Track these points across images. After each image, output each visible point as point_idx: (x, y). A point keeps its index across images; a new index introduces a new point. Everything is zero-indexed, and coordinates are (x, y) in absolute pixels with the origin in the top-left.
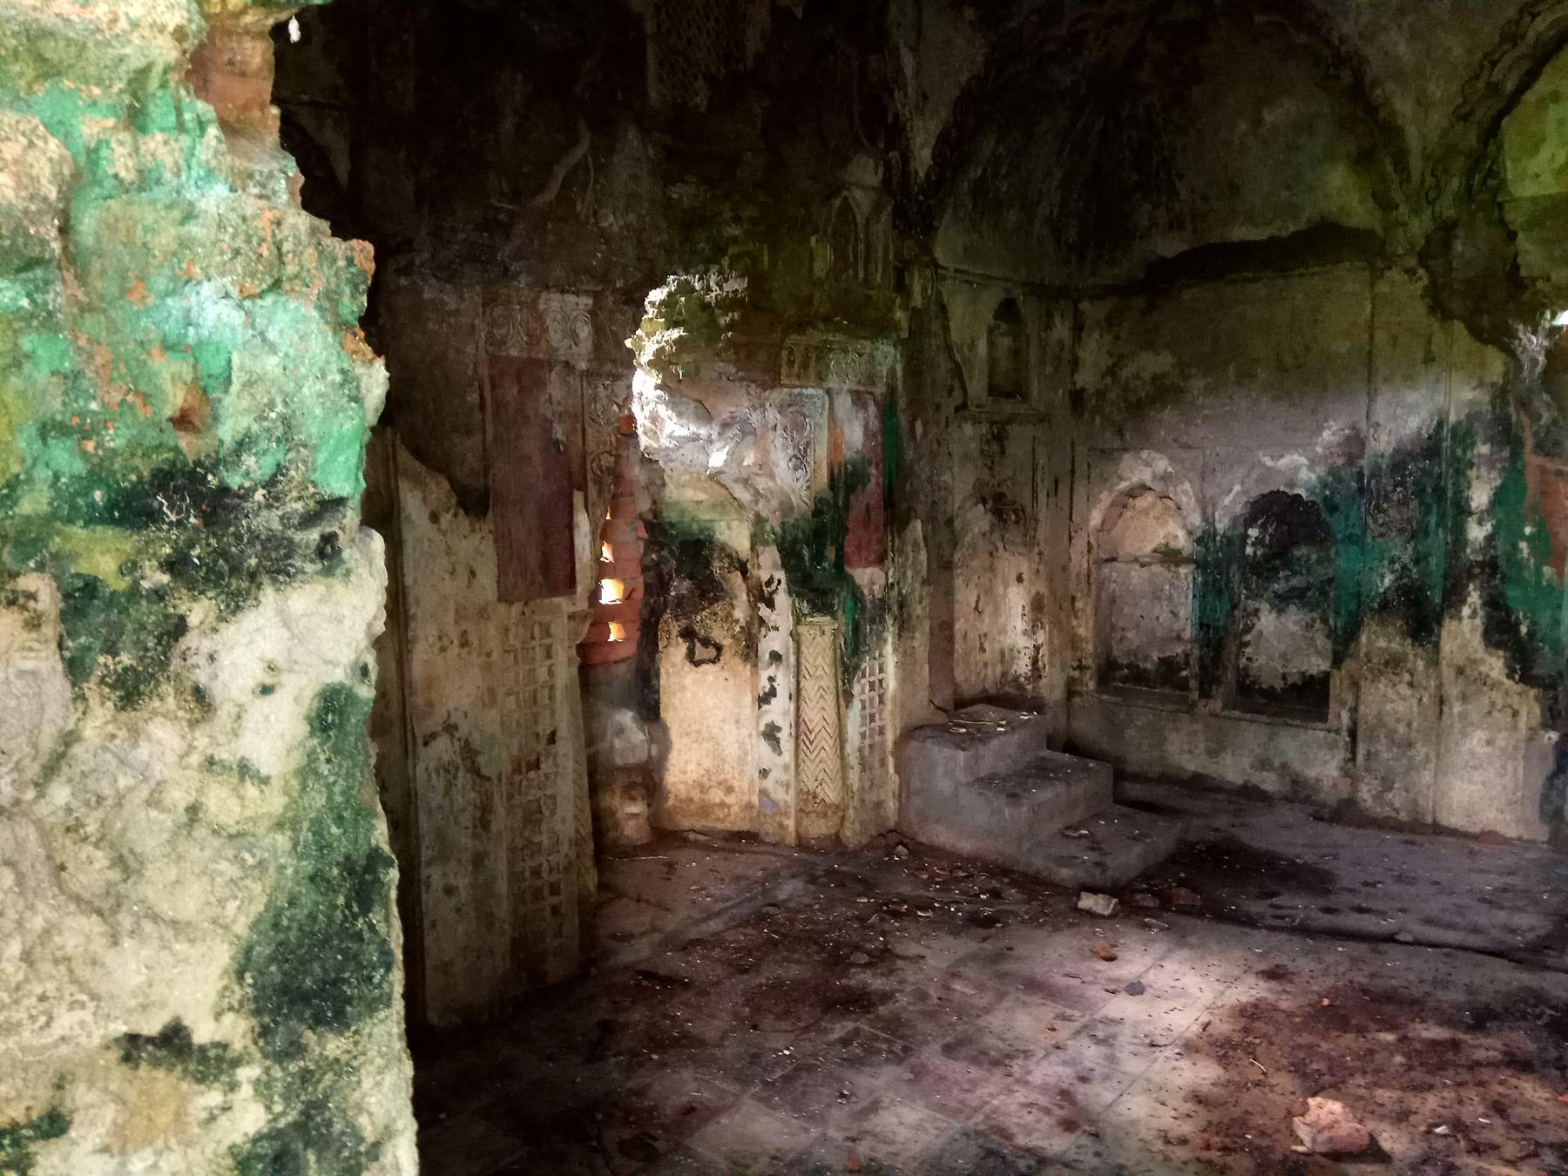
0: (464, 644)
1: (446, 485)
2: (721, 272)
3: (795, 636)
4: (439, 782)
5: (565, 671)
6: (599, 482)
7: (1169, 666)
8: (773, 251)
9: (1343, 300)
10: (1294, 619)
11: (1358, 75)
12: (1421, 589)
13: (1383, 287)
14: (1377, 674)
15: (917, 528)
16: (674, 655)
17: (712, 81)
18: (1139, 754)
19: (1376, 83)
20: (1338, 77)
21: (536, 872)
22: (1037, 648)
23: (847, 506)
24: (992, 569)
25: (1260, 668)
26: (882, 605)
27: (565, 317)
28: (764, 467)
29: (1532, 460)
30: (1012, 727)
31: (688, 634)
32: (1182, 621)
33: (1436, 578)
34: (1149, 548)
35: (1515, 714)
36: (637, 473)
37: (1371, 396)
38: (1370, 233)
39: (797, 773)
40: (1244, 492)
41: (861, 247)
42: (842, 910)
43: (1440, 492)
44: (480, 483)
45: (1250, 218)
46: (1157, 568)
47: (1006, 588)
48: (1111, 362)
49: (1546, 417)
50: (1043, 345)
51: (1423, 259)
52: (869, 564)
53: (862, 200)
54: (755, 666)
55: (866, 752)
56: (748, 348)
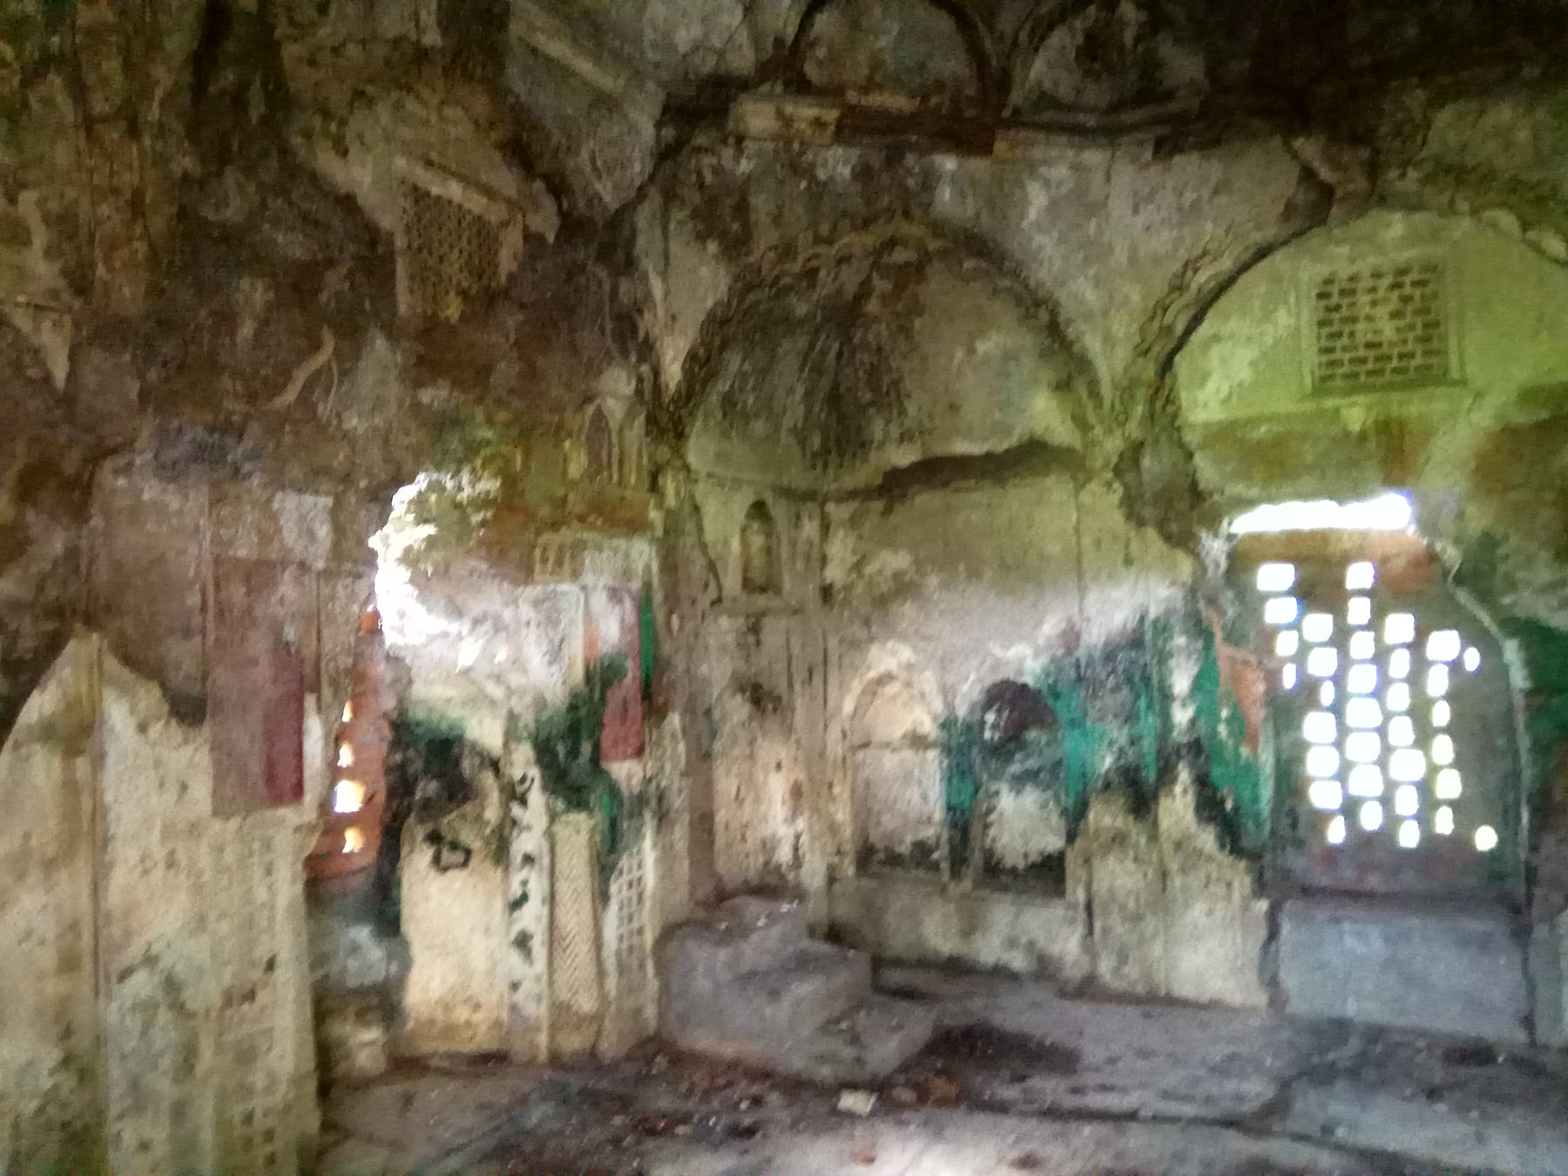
0: (171, 864)
1: (156, 692)
2: (473, 471)
3: (550, 835)
4: (134, 1024)
5: (287, 887)
6: (335, 683)
7: (922, 850)
8: (527, 455)
9: (1053, 511)
10: (1031, 798)
11: (1054, 314)
12: (1137, 769)
13: (1086, 497)
14: (1106, 850)
15: (675, 720)
16: (417, 862)
17: (463, 294)
18: (898, 941)
19: (1069, 322)
20: (1036, 317)
21: (248, 1118)
22: (798, 837)
23: (603, 699)
24: (751, 757)
25: (1004, 847)
26: (641, 800)
27: (303, 518)
28: (517, 662)
29: (1222, 650)
30: (773, 919)
31: (435, 838)
32: (931, 804)
33: (1150, 759)
34: (898, 734)
35: (1229, 885)
36: (381, 670)
37: (1082, 591)
38: (1070, 451)
39: (551, 983)
40: (980, 680)
41: (616, 451)
42: (596, 1134)
43: (1146, 680)
44: (195, 689)
45: (969, 435)
46: (908, 754)
47: (766, 776)
48: (855, 559)
49: (1231, 612)
50: (793, 543)
51: (1118, 472)
52: (625, 757)
53: (615, 409)
54: (506, 869)
55: (625, 954)
56: (511, 540)
